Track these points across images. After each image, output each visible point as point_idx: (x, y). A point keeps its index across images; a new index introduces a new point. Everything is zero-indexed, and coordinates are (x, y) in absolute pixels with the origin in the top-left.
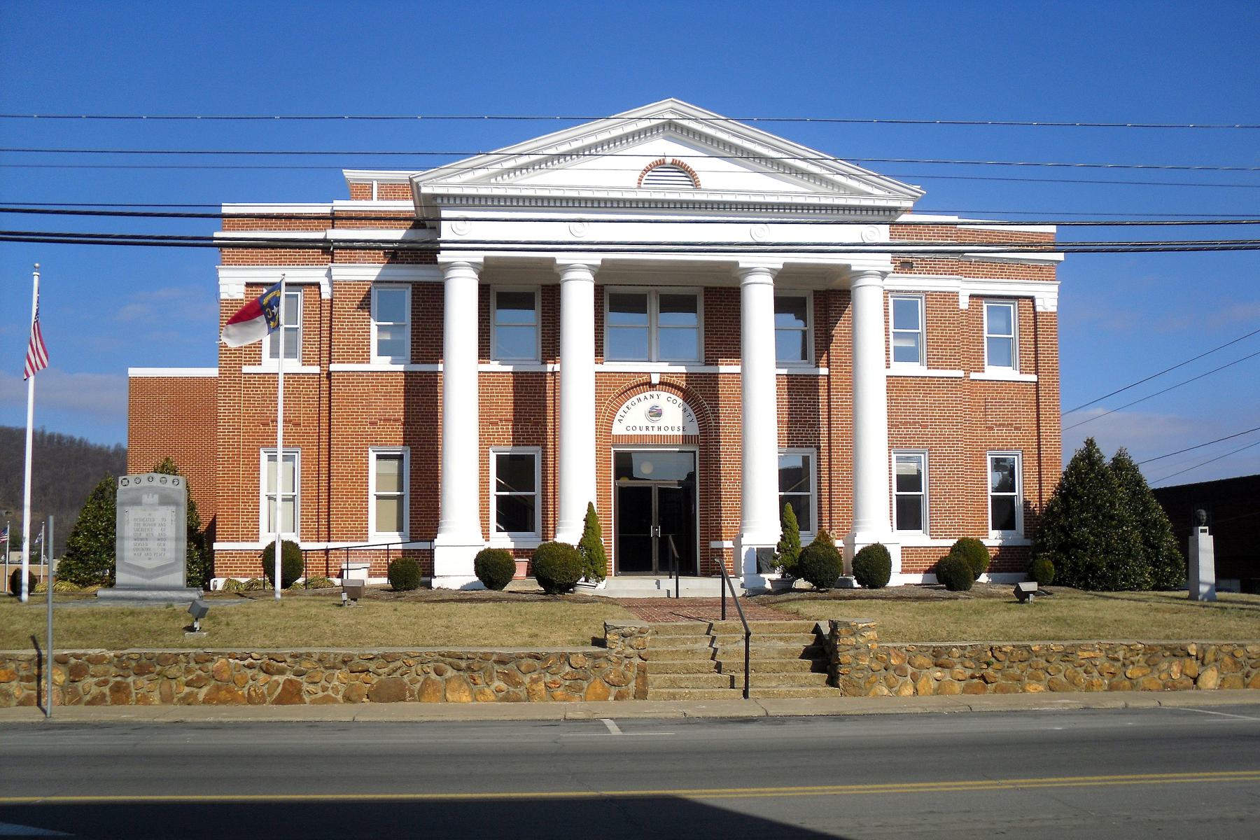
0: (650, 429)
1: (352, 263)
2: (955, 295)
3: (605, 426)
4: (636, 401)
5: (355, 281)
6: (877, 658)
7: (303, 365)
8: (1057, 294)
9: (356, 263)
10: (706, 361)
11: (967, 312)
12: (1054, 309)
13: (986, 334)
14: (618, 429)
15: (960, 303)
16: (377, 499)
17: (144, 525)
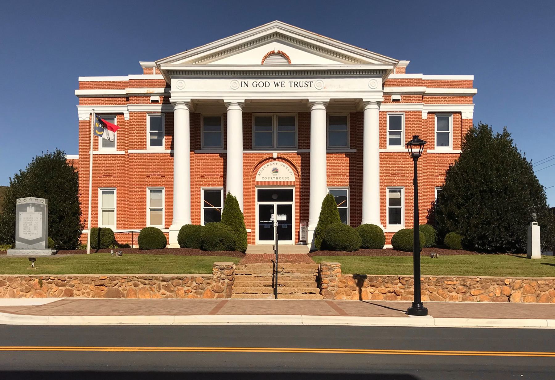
0: (273, 178)
1: (138, 104)
2: (420, 112)
3: (253, 177)
4: (267, 166)
5: (139, 112)
6: (341, 282)
7: (117, 150)
8: (473, 110)
9: (139, 104)
10: (298, 147)
11: (426, 120)
12: (472, 118)
13: (436, 131)
14: (259, 178)
15: (423, 116)
16: (151, 211)
17: (28, 220)
